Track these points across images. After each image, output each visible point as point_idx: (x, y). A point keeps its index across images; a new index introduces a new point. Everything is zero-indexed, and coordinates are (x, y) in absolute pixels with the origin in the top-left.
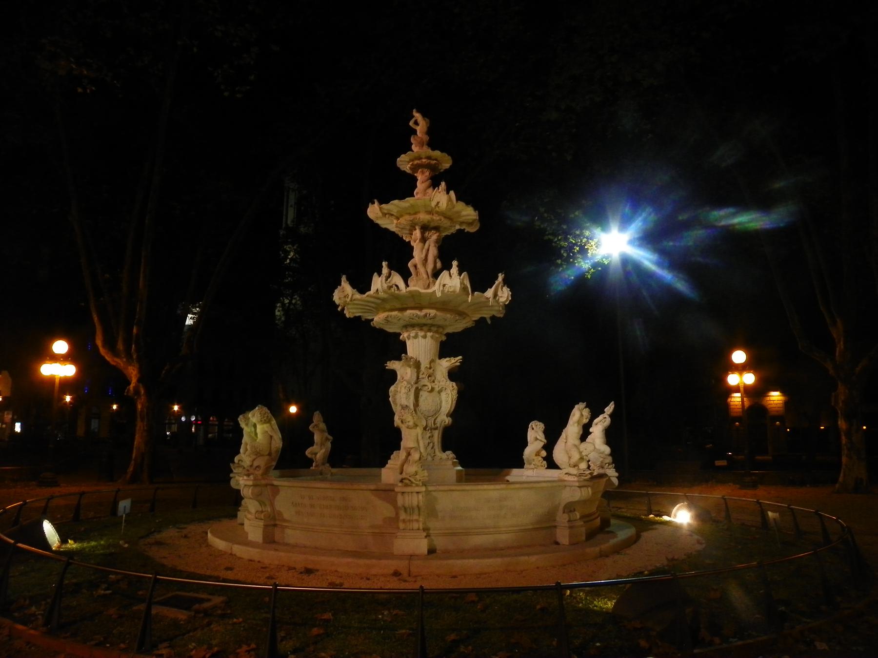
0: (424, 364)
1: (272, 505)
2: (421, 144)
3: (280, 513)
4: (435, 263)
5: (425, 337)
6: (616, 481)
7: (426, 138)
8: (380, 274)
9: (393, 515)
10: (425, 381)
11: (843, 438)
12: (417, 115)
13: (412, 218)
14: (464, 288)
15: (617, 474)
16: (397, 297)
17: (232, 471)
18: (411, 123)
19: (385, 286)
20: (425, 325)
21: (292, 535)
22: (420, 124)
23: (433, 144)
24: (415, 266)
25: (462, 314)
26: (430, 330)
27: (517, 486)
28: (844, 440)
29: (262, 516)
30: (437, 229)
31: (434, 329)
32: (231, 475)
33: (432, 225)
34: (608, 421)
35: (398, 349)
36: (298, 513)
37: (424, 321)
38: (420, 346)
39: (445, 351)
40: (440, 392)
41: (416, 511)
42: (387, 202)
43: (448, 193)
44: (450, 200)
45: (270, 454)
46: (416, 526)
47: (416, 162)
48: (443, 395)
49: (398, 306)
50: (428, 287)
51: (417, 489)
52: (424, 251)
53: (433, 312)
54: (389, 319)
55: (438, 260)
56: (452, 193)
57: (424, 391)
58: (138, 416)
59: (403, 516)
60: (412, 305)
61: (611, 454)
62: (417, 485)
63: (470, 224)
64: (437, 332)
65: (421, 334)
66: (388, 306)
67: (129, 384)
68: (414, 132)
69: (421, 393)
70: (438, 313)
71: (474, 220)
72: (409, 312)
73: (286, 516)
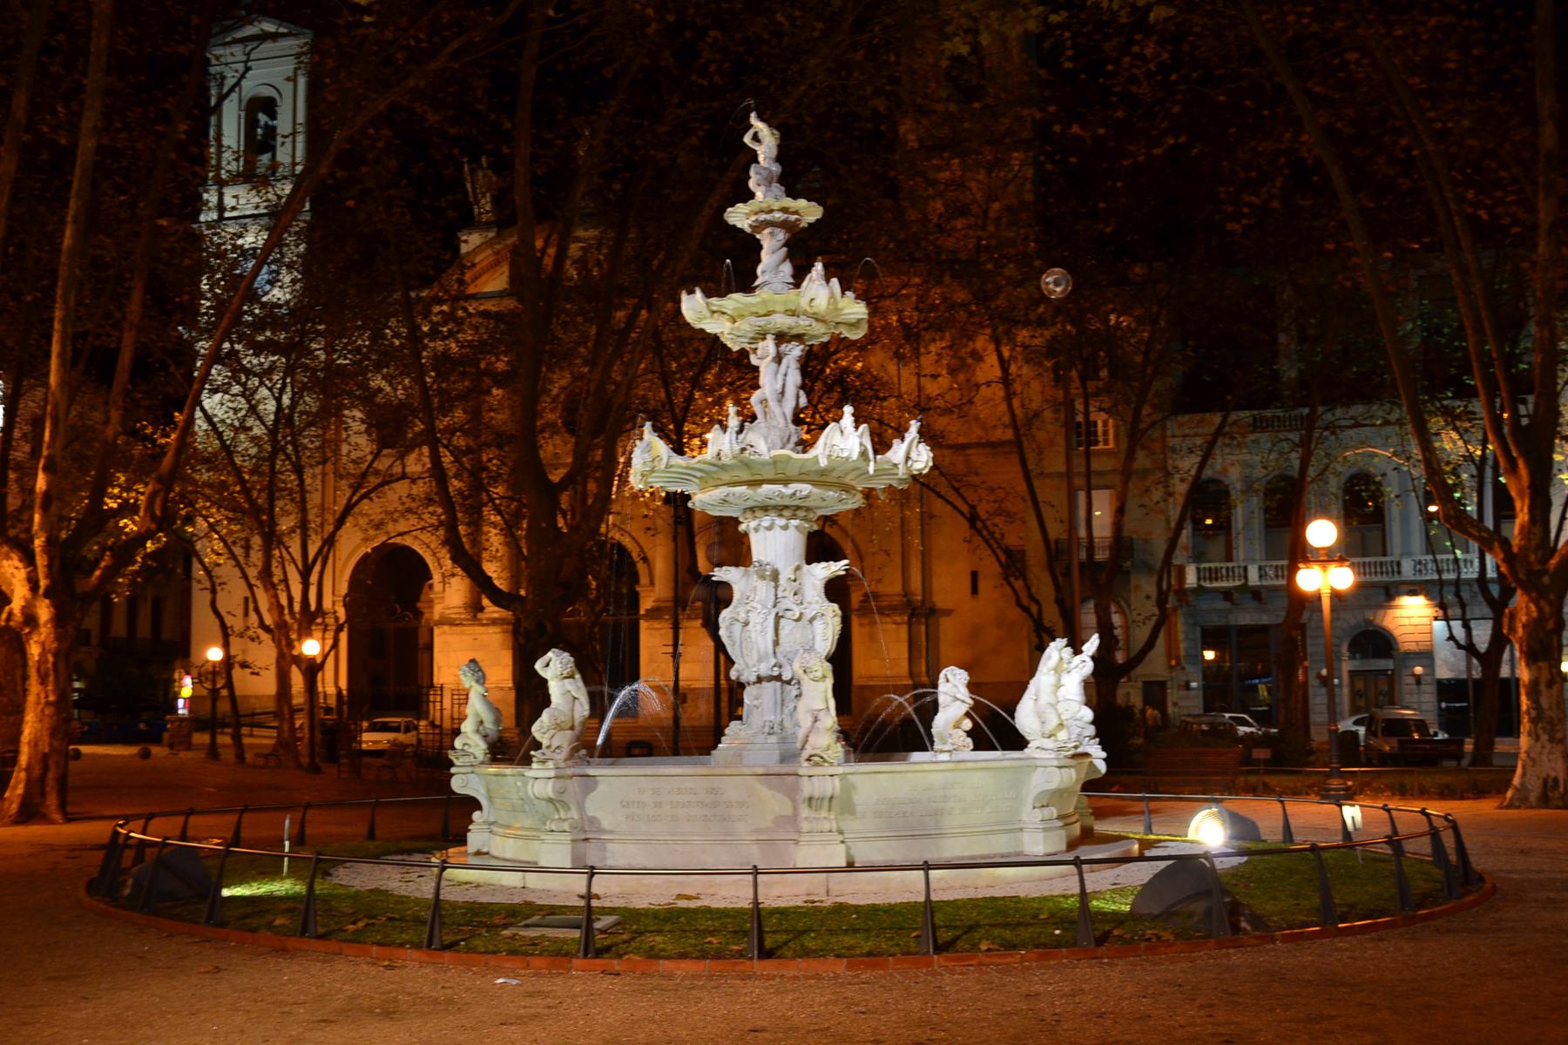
0: (786, 573)
1: (581, 808)
2: (768, 182)
3: (593, 821)
4: (798, 397)
5: (785, 528)
6: (1102, 767)
7: (776, 169)
8: (724, 428)
9: (788, 811)
10: (788, 603)
11: (1524, 699)
12: (757, 124)
13: (762, 321)
14: (863, 454)
15: (1104, 755)
16: (747, 464)
17: (452, 764)
18: (747, 139)
19: (737, 448)
20: (786, 507)
21: (618, 854)
22: (763, 140)
23: (791, 183)
24: (764, 401)
25: (847, 489)
26: (794, 517)
27: (970, 765)
28: (1525, 702)
29: (566, 826)
30: (799, 338)
31: (801, 513)
32: (453, 770)
33: (795, 332)
34: (1089, 666)
35: (736, 549)
36: (629, 817)
37: (787, 502)
38: (775, 543)
39: (819, 547)
40: (811, 621)
41: (826, 803)
42: (722, 295)
43: (828, 281)
44: (832, 296)
45: (572, 728)
46: (826, 826)
47: (762, 217)
48: (818, 624)
49: (745, 476)
50: (805, 445)
51: (832, 770)
52: (780, 377)
53: (805, 489)
54: (730, 499)
55: (802, 393)
56: (835, 281)
57: (780, 616)
58: (33, 673)
59: (805, 812)
60: (771, 476)
61: (1093, 723)
62: (831, 764)
63: (855, 325)
64: (805, 519)
65: (781, 522)
66: (726, 477)
67: (8, 601)
68: (753, 157)
69: (783, 622)
70: (815, 490)
71: (859, 321)
72: (766, 487)
73: (606, 824)
